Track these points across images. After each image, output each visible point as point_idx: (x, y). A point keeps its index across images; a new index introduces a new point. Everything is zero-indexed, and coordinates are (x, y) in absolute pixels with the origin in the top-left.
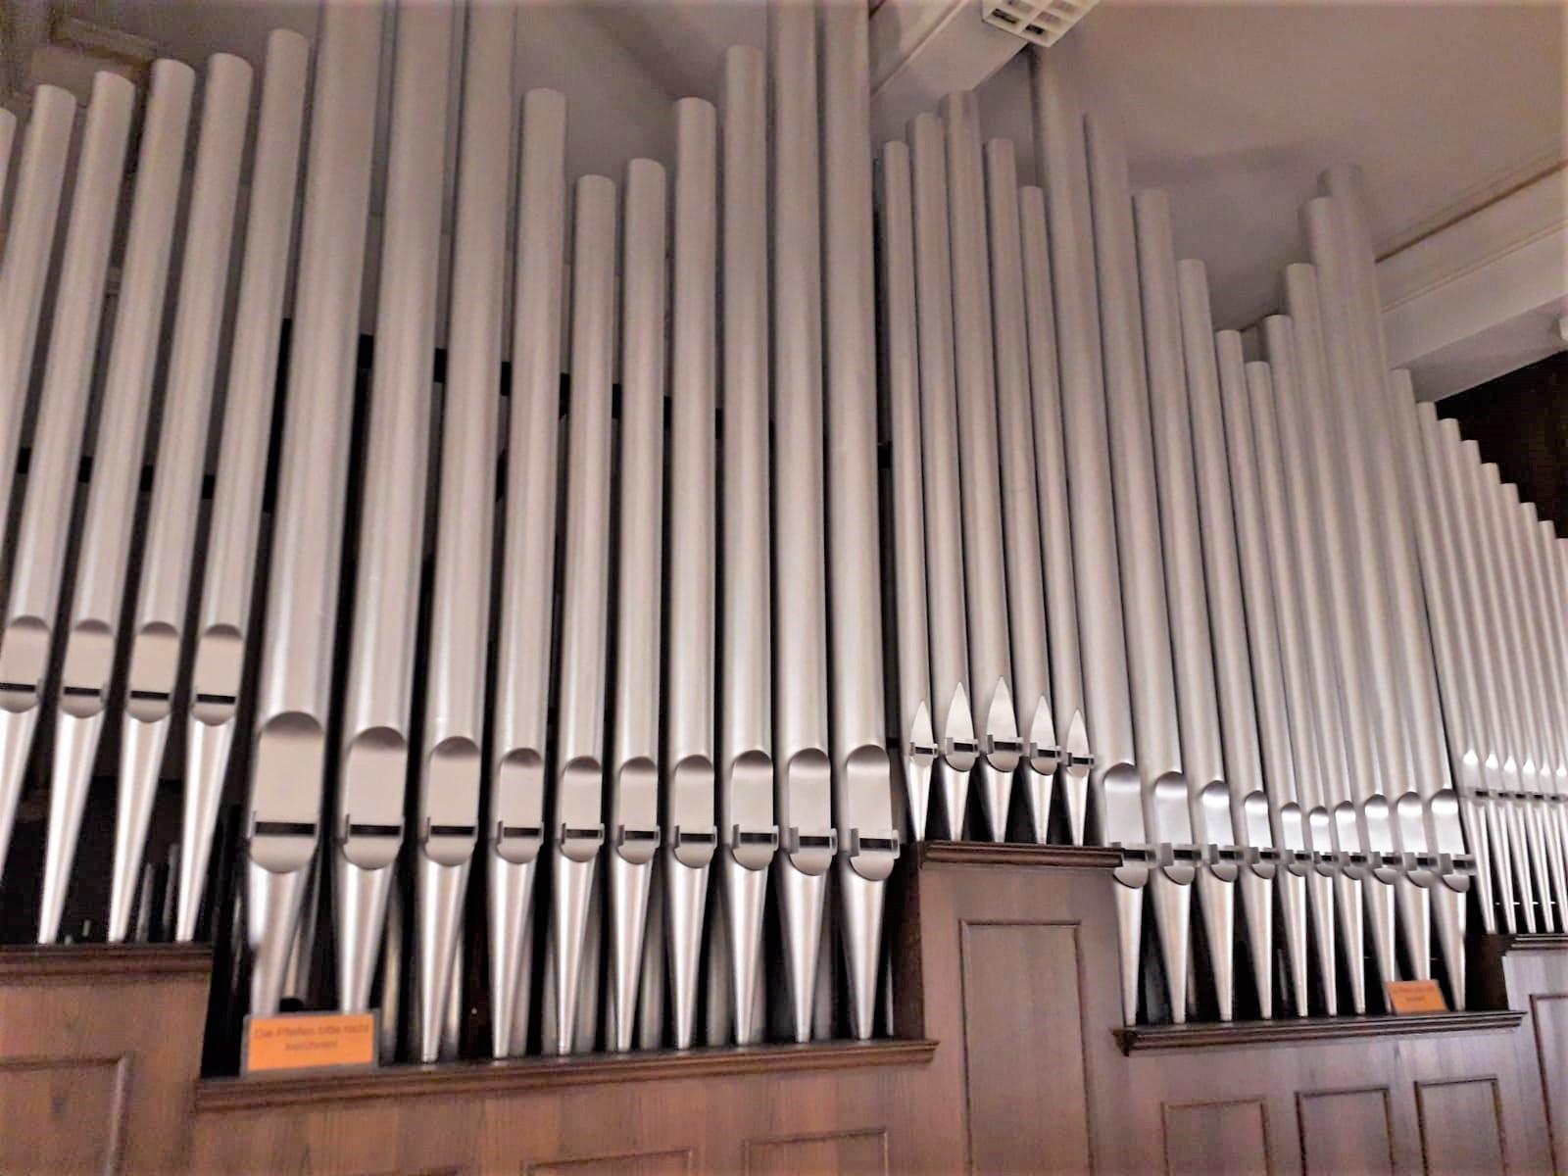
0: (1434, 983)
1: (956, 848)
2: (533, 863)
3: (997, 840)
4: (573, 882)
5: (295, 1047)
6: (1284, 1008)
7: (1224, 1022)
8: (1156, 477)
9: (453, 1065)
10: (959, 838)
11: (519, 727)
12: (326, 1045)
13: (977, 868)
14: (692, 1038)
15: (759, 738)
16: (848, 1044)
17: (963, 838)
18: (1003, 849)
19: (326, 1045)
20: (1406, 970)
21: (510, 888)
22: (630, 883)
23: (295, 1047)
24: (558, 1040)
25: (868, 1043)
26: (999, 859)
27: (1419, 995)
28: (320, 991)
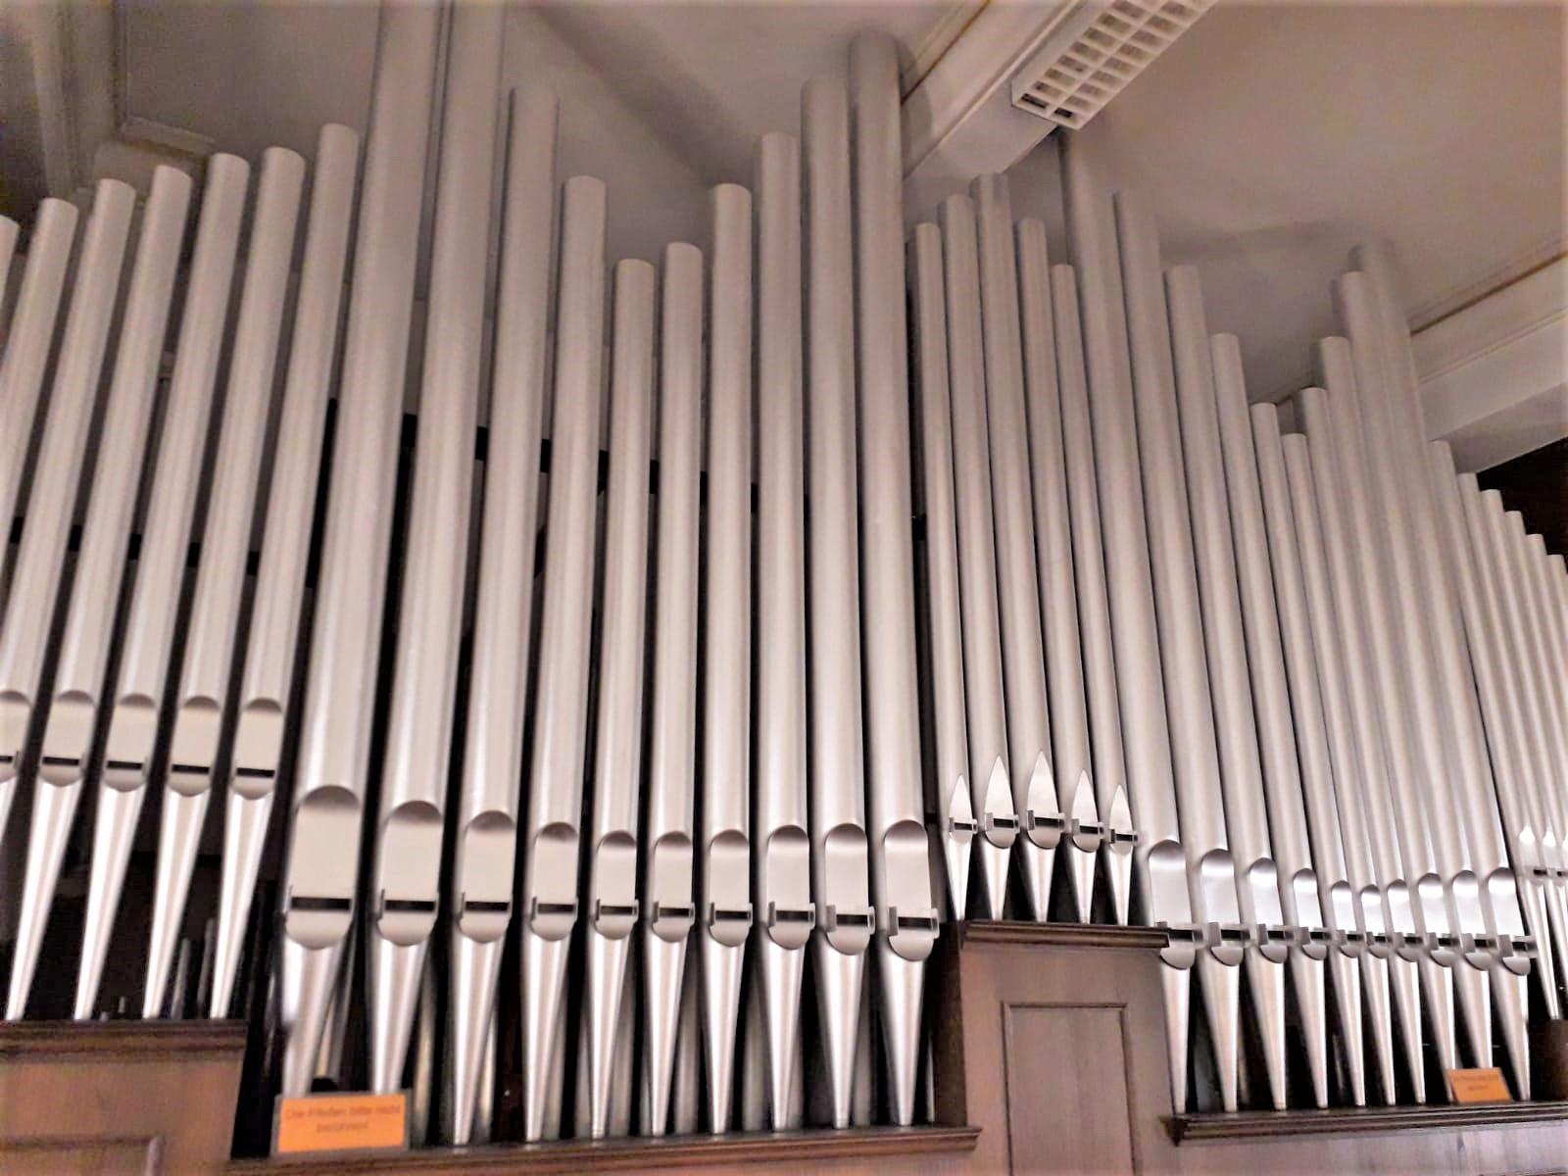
0: (1497, 1071)
2: (567, 941)
4: (607, 960)
7: (1228, 1112)
12: (355, 1127)
13: (1020, 948)
15: (853, 810)
16: (886, 1131)
17: (1005, 917)
19: (355, 1127)
22: (665, 962)
26: (1040, 940)
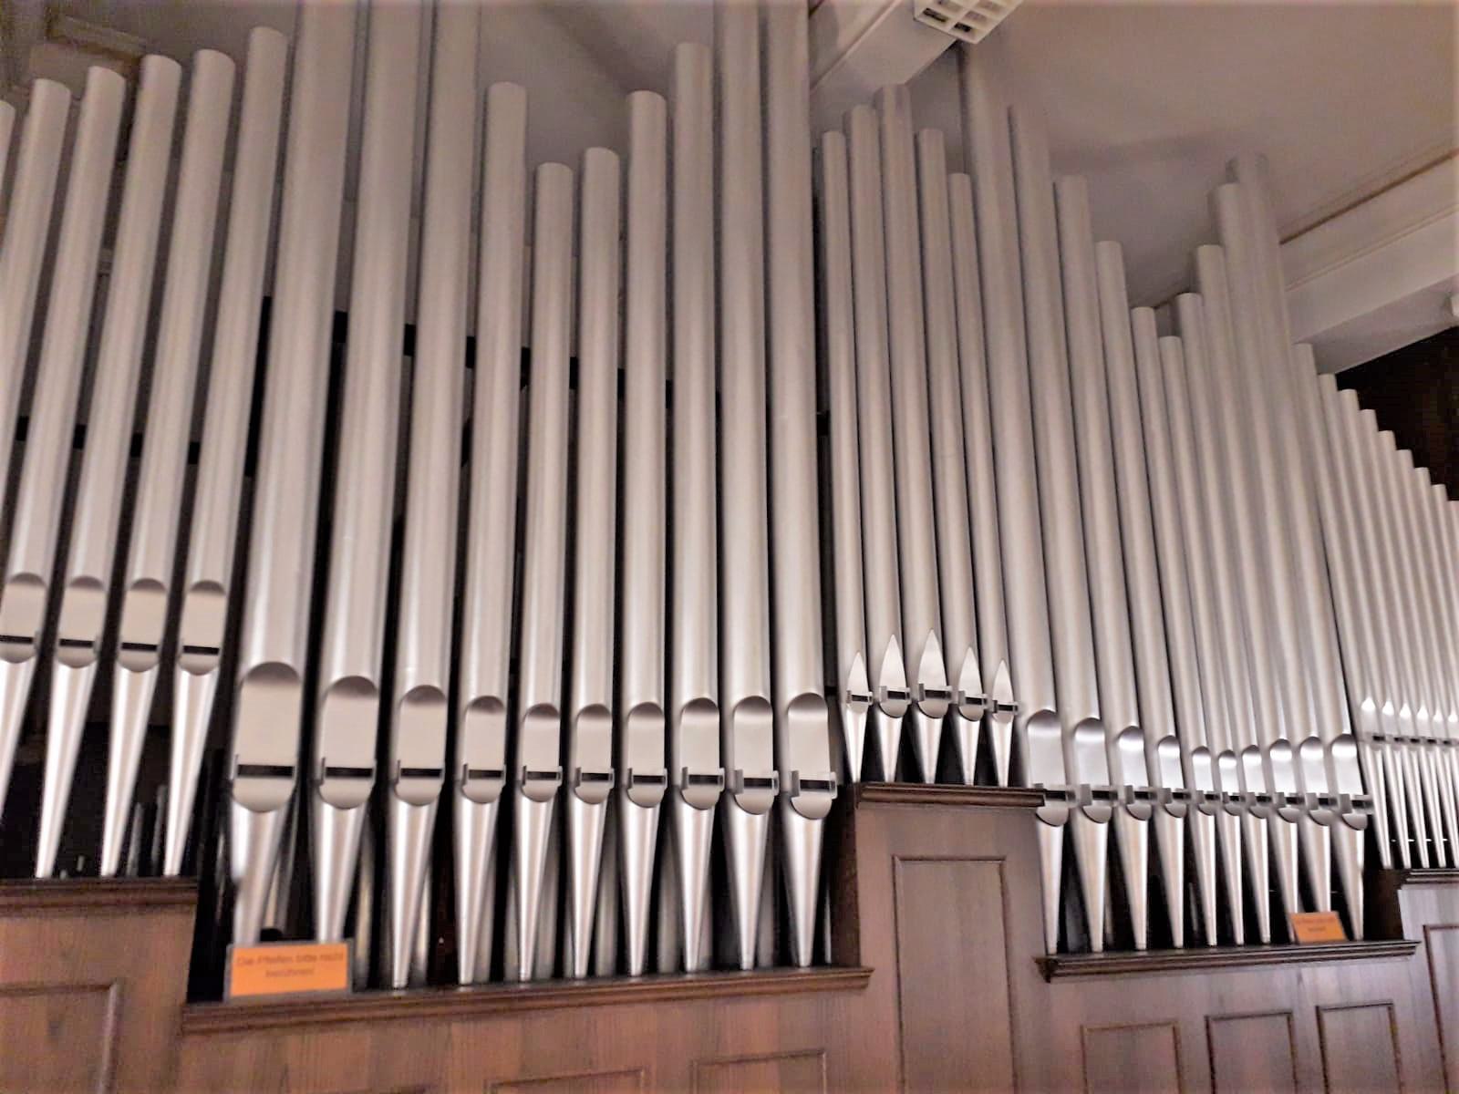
0: (1335, 914)
1: (890, 789)
2: (496, 803)
3: (927, 782)
4: (533, 821)
5: (275, 974)
6: (1195, 937)
7: (1139, 950)
8: (1076, 443)
9: (422, 991)
10: (892, 780)
11: (483, 676)
12: (304, 972)
13: (910, 808)
14: (644, 966)
15: (706, 686)
16: (789, 971)
17: (896, 779)
18: (933, 790)
19: (304, 972)
20: (1308, 902)
21: (474, 826)
22: (586, 822)
23: (275, 974)
24: (519, 967)
25: (808, 971)
26: (930, 799)
27: (1320, 925)
28: (298, 922)
